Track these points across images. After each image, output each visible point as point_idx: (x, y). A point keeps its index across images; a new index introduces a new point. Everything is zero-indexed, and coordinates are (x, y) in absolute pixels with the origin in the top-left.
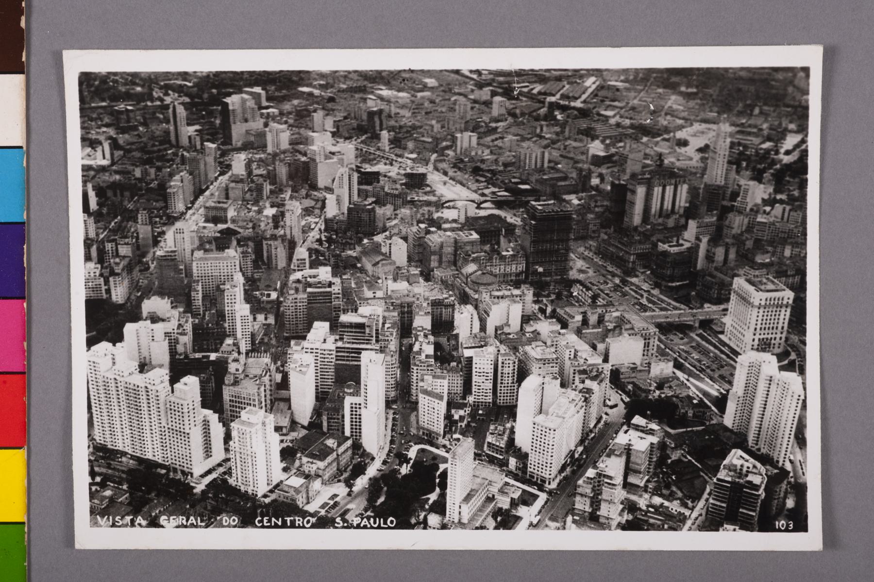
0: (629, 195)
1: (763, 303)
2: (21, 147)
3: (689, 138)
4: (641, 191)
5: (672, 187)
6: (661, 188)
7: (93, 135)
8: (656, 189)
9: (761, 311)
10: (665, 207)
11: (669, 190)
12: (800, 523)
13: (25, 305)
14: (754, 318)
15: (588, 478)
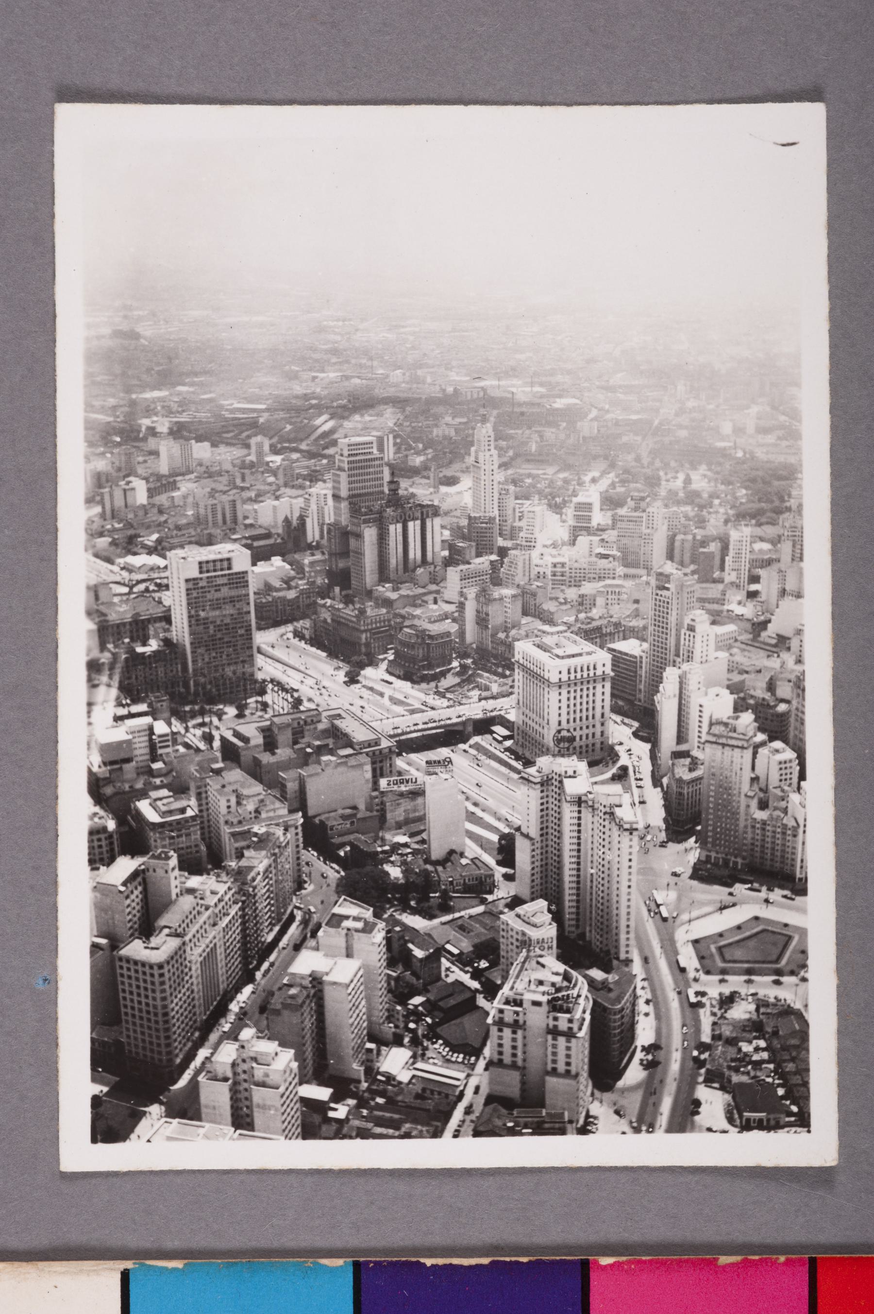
0: (353, 542)
1: (565, 677)
2: (125, 1276)
3: (458, 474)
4: (370, 534)
5: (418, 522)
6: (399, 526)
7: (801, 956)
8: (392, 528)
9: (564, 692)
10: (411, 555)
11: (414, 527)
12: (109, 1127)
13: (605, 1261)
14: (554, 705)
15: (644, 1049)
